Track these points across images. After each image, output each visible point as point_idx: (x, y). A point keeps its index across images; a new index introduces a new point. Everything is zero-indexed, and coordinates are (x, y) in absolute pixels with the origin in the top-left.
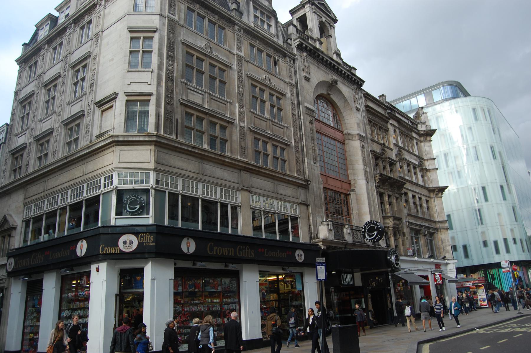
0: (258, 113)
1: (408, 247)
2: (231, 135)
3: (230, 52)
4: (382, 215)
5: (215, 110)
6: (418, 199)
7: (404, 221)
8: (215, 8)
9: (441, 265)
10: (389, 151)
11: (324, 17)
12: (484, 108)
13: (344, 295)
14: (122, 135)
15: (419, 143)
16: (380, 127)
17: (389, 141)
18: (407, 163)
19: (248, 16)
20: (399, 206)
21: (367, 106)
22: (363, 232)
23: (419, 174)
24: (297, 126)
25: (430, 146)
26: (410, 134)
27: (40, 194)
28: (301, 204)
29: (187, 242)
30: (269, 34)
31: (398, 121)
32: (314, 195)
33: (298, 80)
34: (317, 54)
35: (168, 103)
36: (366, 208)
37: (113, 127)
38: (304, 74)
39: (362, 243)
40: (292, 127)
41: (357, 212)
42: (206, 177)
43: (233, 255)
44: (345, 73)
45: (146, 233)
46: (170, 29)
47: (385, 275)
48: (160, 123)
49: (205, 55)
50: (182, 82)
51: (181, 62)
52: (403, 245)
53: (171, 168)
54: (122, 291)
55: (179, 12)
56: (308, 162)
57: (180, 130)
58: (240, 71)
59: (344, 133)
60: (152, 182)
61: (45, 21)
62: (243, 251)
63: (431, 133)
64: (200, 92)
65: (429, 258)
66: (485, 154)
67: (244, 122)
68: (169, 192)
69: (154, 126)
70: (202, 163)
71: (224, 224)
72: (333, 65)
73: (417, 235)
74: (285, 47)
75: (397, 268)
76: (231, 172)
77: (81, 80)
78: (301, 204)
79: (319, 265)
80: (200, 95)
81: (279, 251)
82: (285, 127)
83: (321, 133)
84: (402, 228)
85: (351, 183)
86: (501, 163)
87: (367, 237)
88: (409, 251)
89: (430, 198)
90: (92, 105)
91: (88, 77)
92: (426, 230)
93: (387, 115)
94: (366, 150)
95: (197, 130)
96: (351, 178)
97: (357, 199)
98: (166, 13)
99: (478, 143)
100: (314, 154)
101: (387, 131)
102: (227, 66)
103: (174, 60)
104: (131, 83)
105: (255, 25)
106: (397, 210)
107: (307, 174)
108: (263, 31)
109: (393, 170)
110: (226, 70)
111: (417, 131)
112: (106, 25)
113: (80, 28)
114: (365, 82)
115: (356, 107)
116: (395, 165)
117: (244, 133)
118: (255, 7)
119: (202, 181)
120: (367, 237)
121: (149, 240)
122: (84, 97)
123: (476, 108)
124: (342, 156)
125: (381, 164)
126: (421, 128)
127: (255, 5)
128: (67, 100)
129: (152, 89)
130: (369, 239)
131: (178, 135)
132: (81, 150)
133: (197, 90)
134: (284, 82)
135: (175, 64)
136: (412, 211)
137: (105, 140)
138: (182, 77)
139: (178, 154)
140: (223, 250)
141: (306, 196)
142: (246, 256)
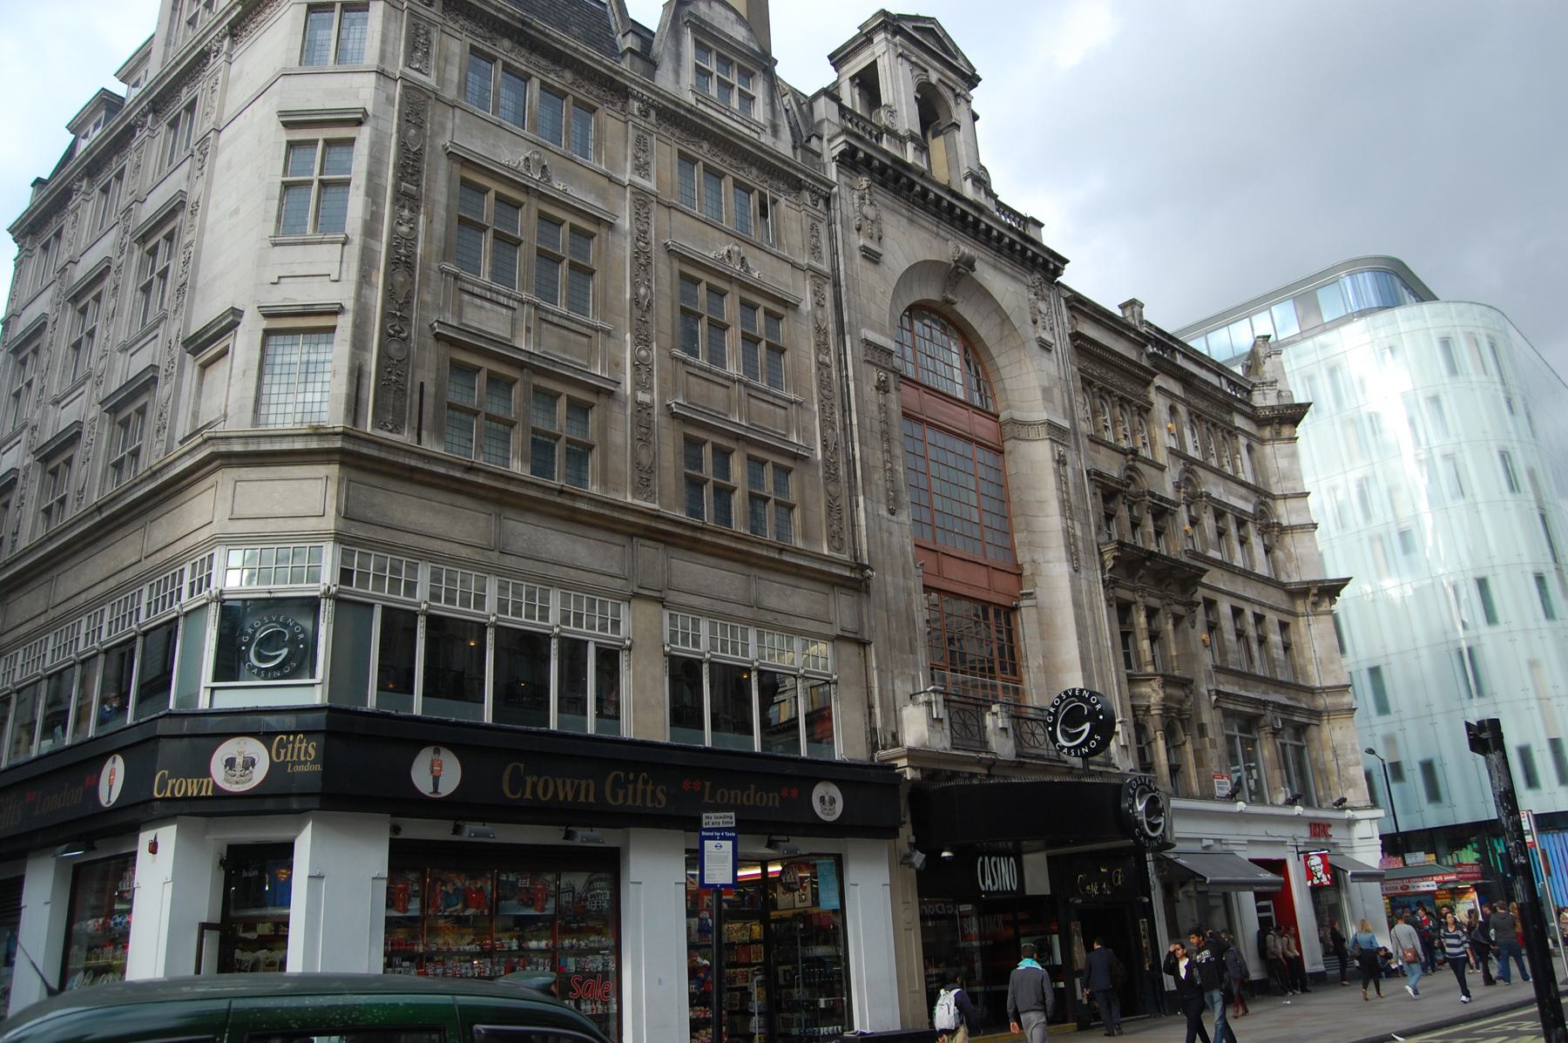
0: (702, 361)
1: (1217, 769)
2: (604, 430)
3: (610, 179)
4: (1123, 671)
5: (551, 355)
6: (1251, 620)
7: (1203, 690)
8: (562, 48)
9: (1330, 826)
10: (1154, 472)
11: (935, 69)
12: (1478, 337)
13: (1000, 922)
14: (241, 434)
15: (1255, 445)
16: (1121, 398)
17: (1150, 442)
18: (1215, 509)
19: (677, 73)
20: (1184, 641)
21: (1076, 336)
22: (1049, 724)
23: (1256, 543)
24: (834, 397)
25: (1294, 456)
26: (1227, 418)
27: (36, 620)
28: (839, 638)
29: (432, 761)
30: (745, 123)
31: (1185, 379)
32: (887, 611)
33: (841, 259)
34: (904, 180)
35: (391, 336)
36: (1069, 649)
37: (223, 412)
38: (861, 242)
39: (1050, 760)
40: (816, 401)
41: (1041, 662)
42: (513, 558)
43: (591, 799)
44: (1001, 236)
45: (295, 733)
46: (407, 115)
47: (1133, 859)
48: (363, 395)
49: (526, 189)
50: (442, 271)
51: (441, 212)
52: (1199, 763)
53: (394, 532)
54: (233, 913)
55: (442, 63)
56: (869, 509)
57: (431, 416)
58: (641, 235)
59: (1002, 419)
60: (328, 577)
61: (93, 111)
62: (627, 789)
63: (1292, 415)
64: (502, 299)
65: (1291, 802)
66: (1484, 477)
67: (651, 388)
68: (383, 607)
69: (343, 406)
70: (498, 516)
71: (573, 701)
72: (958, 211)
73: (1250, 733)
74: (799, 160)
75: (1156, 838)
76: (599, 543)
77: (161, 277)
78: (839, 638)
79: (714, 838)
80: (504, 311)
81: (753, 786)
82: (792, 403)
83: (921, 421)
84: (1197, 705)
85: (1024, 574)
86: (1534, 505)
87: (1062, 741)
88: (1219, 783)
89: (1295, 615)
90: (178, 349)
91: (175, 267)
92: (1279, 715)
93: (1145, 362)
94: (1073, 468)
95: (489, 417)
96: (1023, 556)
97: (1040, 623)
98: (398, 67)
99: (1460, 443)
100: (889, 484)
101: (1148, 411)
102: (598, 221)
103: (418, 207)
104: (280, 277)
105: (700, 98)
106: (1177, 656)
107: (865, 547)
108: (725, 115)
109: (1167, 531)
110: (595, 235)
111: (1249, 410)
112: (229, 111)
113: (169, 124)
114: (1067, 261)
115: (1040, 337)
116: (1172, 514)
117: (651, 422)
118: (699, 45)
119: (499, 571)
120: (1062, 741)
121: (305, 756)
122: (162, 326)
123: (1453, 335)
124: (993, 491)
125: (1123, 512)
126: (1264, 400)
127: (699, 38)
128: (122, 338)
129: (344, 294)
130: (1069, 748)
131: (424, 434)
132: (136, 485)
133: (495, 295)
134: (794, 265)
135: (422, 219)
136: (1231, 657)
137: (195, 453)
138: (445, 256)
139: (417, 489)
140: (556, 787)
141: (860, 615)
142: (639, 802)
